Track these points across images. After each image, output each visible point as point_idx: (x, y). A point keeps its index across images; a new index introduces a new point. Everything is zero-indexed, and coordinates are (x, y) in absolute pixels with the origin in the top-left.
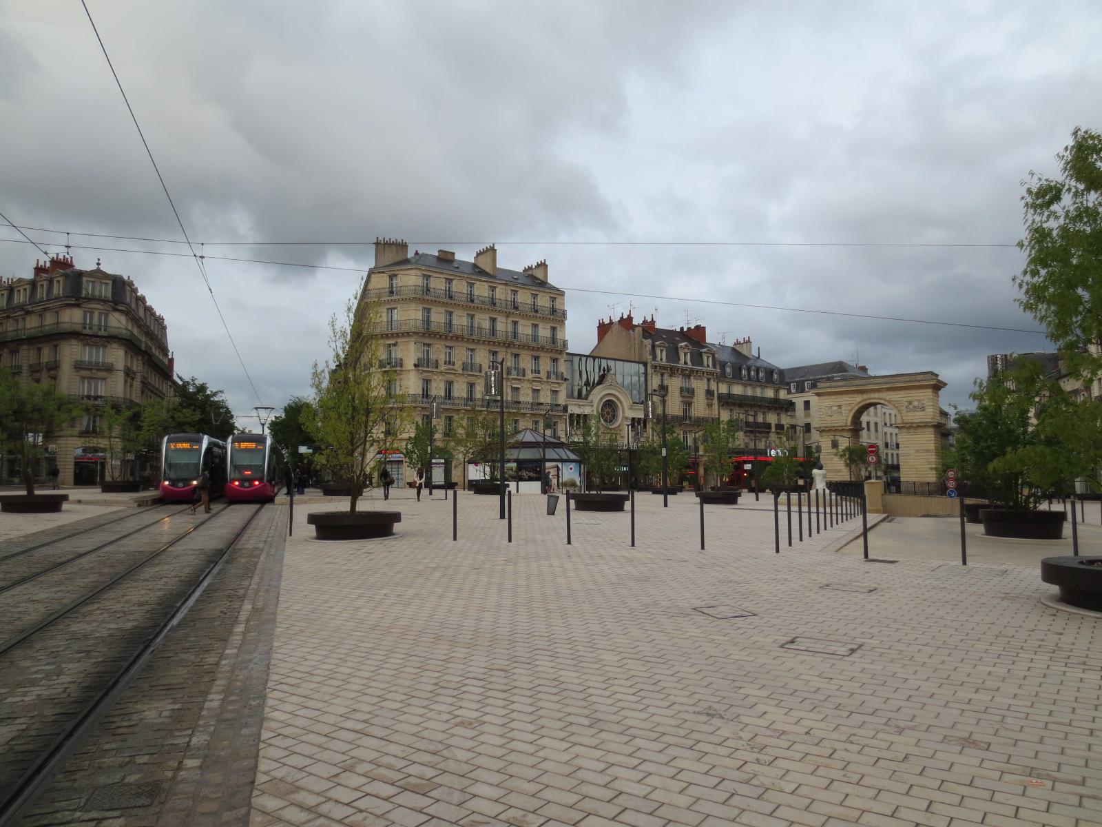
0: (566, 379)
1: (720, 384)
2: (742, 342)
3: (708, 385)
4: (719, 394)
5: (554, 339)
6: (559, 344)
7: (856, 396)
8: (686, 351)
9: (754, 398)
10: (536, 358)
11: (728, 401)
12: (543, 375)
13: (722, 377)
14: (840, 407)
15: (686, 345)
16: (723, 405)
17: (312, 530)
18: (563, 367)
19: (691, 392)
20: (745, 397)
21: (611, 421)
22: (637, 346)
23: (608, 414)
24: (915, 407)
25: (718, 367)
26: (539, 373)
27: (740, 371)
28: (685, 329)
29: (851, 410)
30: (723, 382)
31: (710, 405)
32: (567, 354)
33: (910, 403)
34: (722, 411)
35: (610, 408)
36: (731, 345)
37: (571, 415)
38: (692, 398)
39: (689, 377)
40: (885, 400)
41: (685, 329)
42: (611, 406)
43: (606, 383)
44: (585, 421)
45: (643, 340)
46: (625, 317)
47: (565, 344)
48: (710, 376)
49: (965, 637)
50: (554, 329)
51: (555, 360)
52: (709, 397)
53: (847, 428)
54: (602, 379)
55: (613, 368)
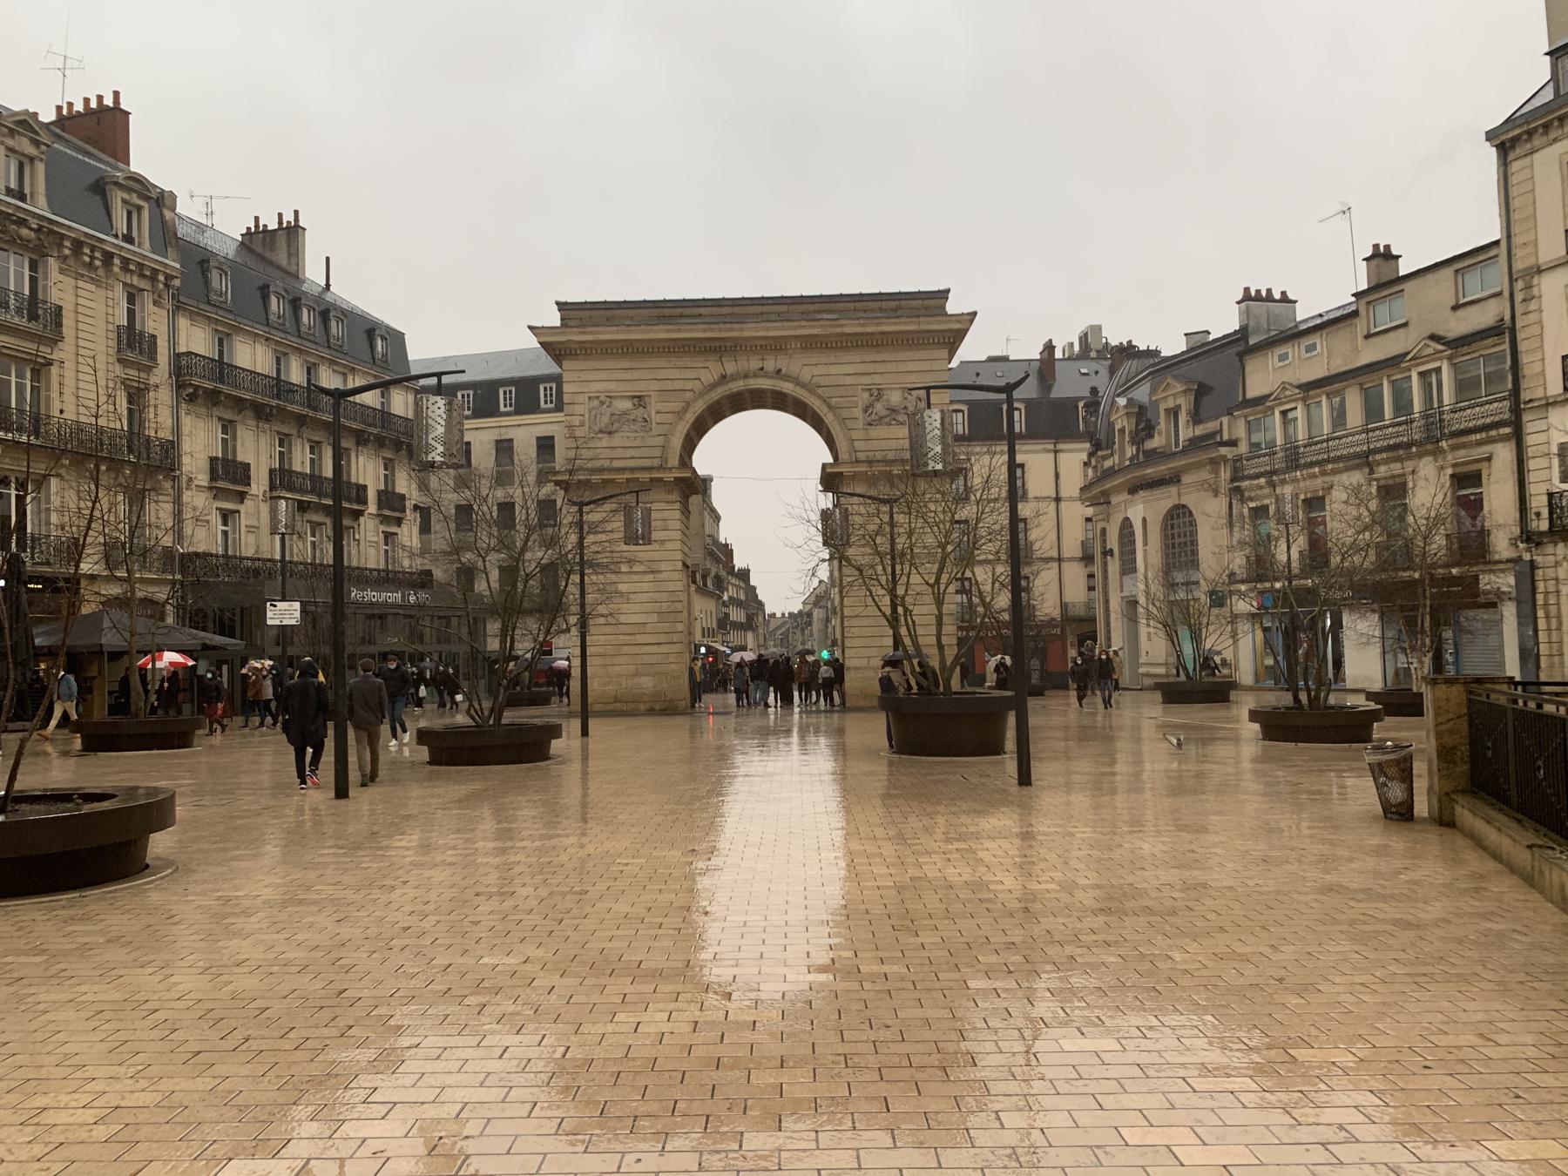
1: (183, 323)
2: (273, 226)
7: (698, 362)
11: (209, 387)
14: (640, 400)
16: (191, 399)
17: (424, 753)
24: (893, 410)
29: (680, 414)
30: (194, 315)
34: (187, 422)
40: (797, 382)
52: (130, 356)
53: (669, 476)
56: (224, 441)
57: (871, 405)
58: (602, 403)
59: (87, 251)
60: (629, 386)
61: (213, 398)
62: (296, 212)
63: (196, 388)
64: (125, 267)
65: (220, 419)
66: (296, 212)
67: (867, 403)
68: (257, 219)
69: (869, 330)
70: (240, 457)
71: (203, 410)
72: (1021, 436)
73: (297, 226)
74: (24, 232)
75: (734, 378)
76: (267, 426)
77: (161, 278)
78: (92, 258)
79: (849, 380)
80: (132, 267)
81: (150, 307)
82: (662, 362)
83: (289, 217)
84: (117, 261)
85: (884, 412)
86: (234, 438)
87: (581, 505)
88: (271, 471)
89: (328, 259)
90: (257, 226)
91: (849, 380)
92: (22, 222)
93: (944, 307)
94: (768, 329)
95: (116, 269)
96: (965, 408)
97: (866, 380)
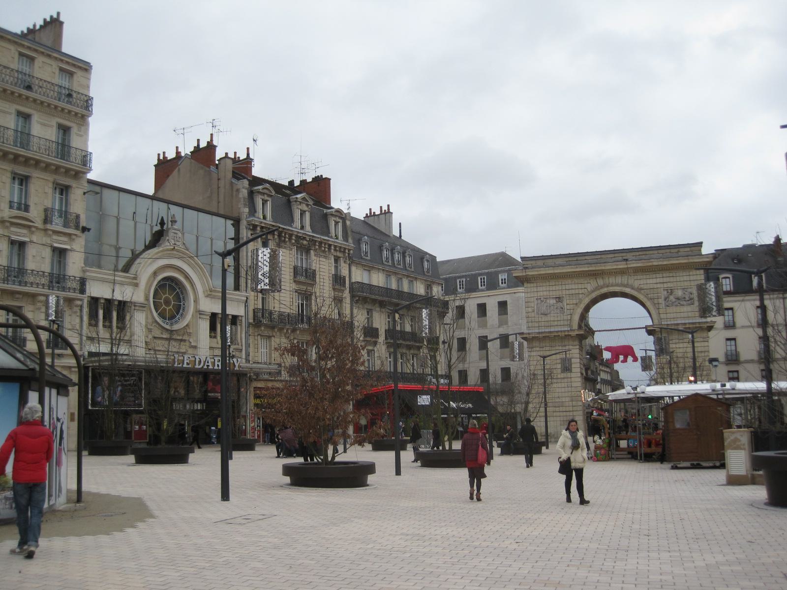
0: (85, 229)
1: (353, 268)
2: (378, 212)
3: (336, 267)
4: (351, 284)
5: (64, 148)
6: (76, 156)
8: (305, 208)
9: (400, 294)
10: (23, 180)
11: (364, 296)
12: (35, 214)
13: (354, 259)
14: (559, 299)
15: (304, 199)
16: (357, 302)
18: (79, 205)
19: (311, 275)
20: (387, 291)
21: (172, 317)
22: (222, 190)
23: (167, 302)
24: (678, 299)
25: (350, 240)
26: (27, 209)
27: (381, 251)
28: (297, 183)
31: (338, 300)
32: (91, 182)
33: (671, 292)
34: (355, 311)
35: (171, 293)
36: (361, 216)
37: (94, 301)
38: (312, 285)
39: (308, 251)
41: (297, 183)
42: (172, 289)
43: (165, 245)
44: (121, 318)
45: (234, 181)
46: (203, 144)
47: (85, 160)
48: (341, 254)
49: (526, 561)
50: (65, 130)
51: (64, 190)
52: (337, 287)
53: (573, 334)
54: (157, 238)
55: (178, 218)
56: (368, 319)
57: (668, 297)
58: (542, 301)
59: (323, 245)
60: (554, 293)
61: (365, 300)
62: (388, 206)
63: (359, 297)
64: (335, 250)
65: (367, 309)
66: (388, 206)
67: (666, 296)
68: (370, 209)
69: (665, 263)
70: (375, 326)
71: (361, 306)
72: (766, 291)
73: (389, 212)
74: (305, 242)
75: (602, 287)
76: (384, 310)
77: (347, 251)
78: (325, 248)
79: (659, 286)
80: (338, 249)
81: (343, 264)
82: (569, 281)
83: (385, 208)
84: (333, 247)
85: (674, 300)
86: (372, 316)
87: (544, 357)
88: (386, 330)
89: (400, 224)
90: (370, 213)
91: (659, 286)
92: (304, 239)
93: (700, 250)
94: (617, 265)
95: (332, 251)
96: (730, 276)
97: (665, 285)
